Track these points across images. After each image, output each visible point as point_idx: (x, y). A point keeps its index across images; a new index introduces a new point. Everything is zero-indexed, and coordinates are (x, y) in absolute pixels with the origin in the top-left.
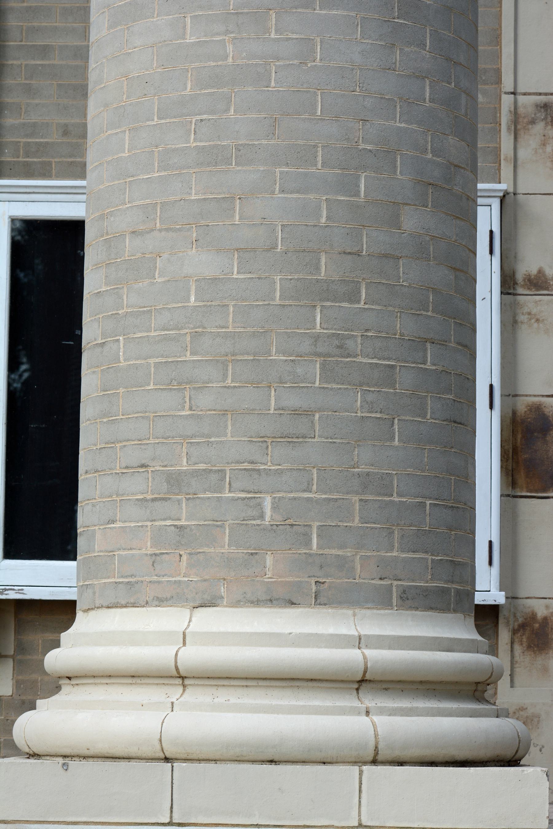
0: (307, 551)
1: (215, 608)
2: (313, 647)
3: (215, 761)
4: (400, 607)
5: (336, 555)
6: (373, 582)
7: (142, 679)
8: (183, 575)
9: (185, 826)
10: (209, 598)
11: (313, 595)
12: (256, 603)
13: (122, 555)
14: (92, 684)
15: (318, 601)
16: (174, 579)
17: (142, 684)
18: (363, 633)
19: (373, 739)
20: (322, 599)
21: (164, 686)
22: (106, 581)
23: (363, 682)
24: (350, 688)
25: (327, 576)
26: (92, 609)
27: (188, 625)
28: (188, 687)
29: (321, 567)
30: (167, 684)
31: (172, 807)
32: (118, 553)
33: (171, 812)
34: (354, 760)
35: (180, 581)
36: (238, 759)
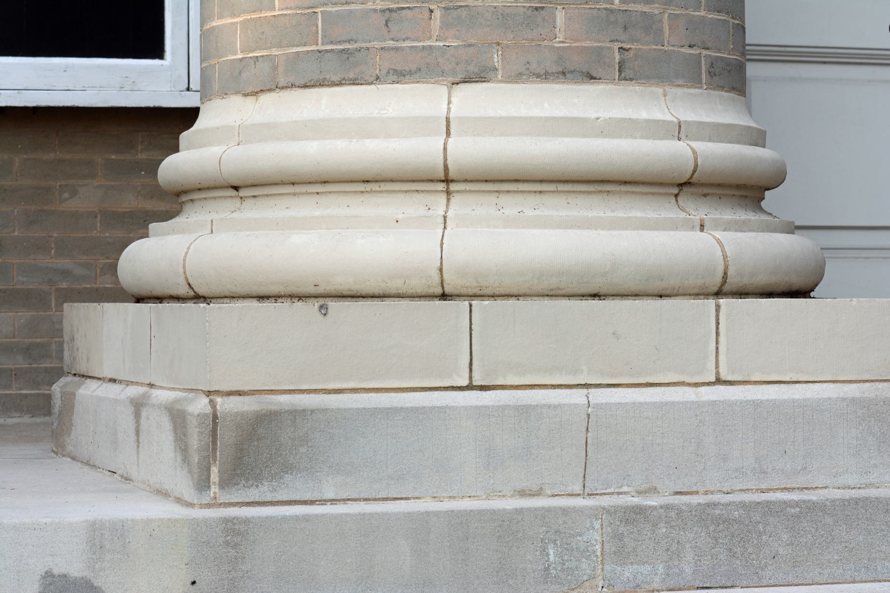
0: (608, 6)
1: (484, 84)
2: (626, 137)
3: (517, 296)
4: (712, 86)
5: (642, 12)
6: (683, 50)
7: (382, 184)
8: (435, 38)
9: (489, 390)
10: (476, 70)
11: (617, 67)
12: (544, 76)
13: (330, 12)
14: (289, 194)
15: (623, 75)
16: (421, 44)
17: (380, 192)
18: (683, 118)
19: (721, 262)
20: (627, 73)
21: (416, 193)
22: (299, 49)
23: (688, 186)
24: (669, 194)
25: (632, 40)
26: (270, 90)
27: (449, 109)
28: (454, 194)
29: (625, 28)
30: (422, 191)
31: (471, 364)
32: (322, 9)
33: (471, 370)
34: (696, 291)
35: (431, 47)
36: (551, 293)
